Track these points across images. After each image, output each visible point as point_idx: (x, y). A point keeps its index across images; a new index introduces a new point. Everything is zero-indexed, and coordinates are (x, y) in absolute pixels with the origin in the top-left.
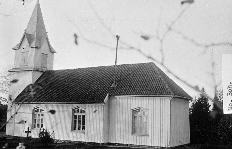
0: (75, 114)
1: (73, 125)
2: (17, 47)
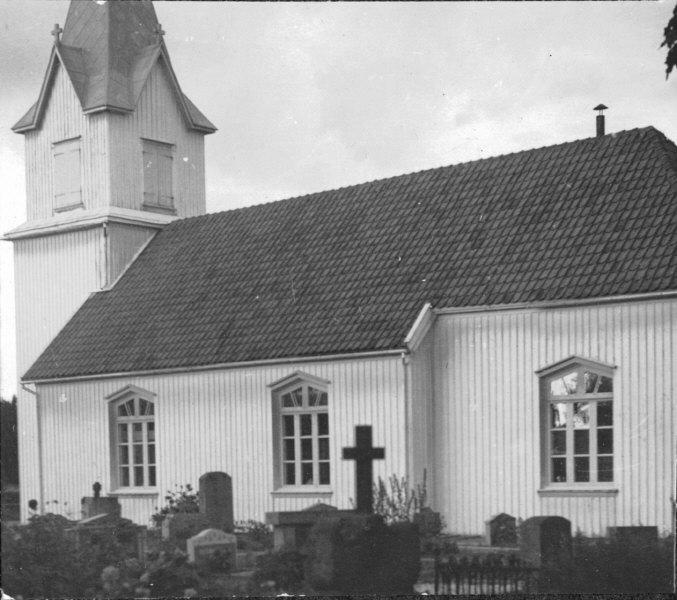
0: (288, 410)
1: (283, 461)
2: (32, 120)
